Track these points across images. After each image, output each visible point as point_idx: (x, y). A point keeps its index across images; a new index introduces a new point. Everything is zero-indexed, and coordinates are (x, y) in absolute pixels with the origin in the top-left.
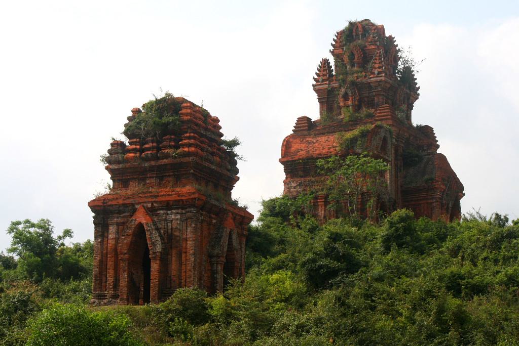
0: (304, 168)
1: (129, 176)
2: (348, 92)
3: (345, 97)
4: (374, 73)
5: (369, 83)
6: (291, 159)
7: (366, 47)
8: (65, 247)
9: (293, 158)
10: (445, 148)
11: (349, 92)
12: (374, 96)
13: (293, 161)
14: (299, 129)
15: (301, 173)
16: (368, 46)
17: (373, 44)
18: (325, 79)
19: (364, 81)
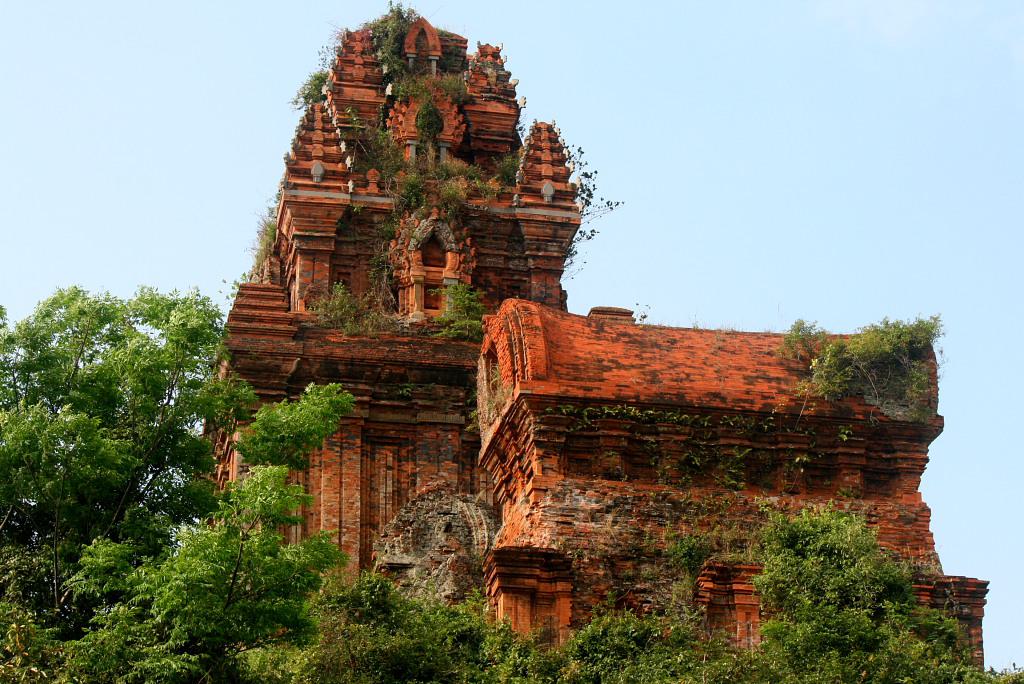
0: (630, 440)
1: (72, 582)
2: (443, 236)
3: (431, 252)
4: (537, 193)
5: (516, 222)
6: (580, 394)
7: (474, 104)
8: (558, 145)
9: (589, 389)
10: (935, 449)
11: (447, 235)
12: (528, 273)
13: (586, 402)
14: (254, 325)
15: (614, 460)
16: (478, 101)
17: (499, 101)
18: (334, 173)
19: (500, 209)
